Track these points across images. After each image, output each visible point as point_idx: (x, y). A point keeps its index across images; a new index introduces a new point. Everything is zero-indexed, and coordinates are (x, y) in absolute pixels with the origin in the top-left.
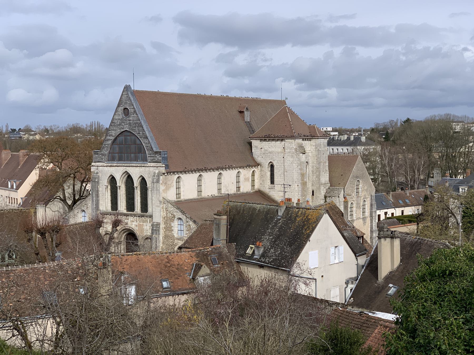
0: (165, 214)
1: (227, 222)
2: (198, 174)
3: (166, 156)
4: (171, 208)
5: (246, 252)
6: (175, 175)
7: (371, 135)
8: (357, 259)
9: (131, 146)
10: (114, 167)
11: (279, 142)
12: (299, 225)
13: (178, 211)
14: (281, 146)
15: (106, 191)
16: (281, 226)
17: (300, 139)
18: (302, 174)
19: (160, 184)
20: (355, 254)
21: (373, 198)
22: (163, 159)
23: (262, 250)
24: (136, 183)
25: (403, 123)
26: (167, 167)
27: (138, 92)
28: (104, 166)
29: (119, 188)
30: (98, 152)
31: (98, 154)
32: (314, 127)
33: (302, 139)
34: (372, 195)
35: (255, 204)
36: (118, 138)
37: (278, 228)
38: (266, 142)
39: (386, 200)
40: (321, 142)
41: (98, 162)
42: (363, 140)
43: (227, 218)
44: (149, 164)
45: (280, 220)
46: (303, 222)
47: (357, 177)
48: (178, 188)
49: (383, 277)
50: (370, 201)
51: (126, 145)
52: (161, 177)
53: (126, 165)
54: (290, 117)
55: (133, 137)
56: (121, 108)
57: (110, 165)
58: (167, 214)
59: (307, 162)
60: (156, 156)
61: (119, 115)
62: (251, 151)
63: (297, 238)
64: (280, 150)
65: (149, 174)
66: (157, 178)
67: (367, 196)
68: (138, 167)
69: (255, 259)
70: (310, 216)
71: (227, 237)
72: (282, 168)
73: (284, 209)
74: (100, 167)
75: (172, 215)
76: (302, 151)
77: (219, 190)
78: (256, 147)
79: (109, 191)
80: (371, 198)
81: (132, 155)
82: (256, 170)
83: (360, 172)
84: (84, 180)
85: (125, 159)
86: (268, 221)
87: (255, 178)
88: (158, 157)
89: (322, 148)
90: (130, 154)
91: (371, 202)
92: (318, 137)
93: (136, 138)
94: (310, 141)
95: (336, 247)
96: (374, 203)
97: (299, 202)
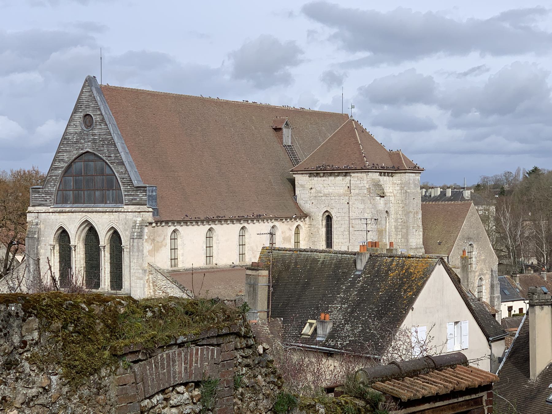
0: (151, 291)
1: (269, 280)
2: (207, 227)
3: (154, 194)
4: (163, 282)
5: (302, 331)
6: (169, 226)
7: (476, 194)
8: (490, 345)
9: (96, 177)
10: (66, 214)
11: (340, 178)
12: (393, 283)
13: (174, 286)
14: (345, 185)
15: (52, 254)
16: (362, 286)
17: (376, 172)
18: (379, 231)
19: (145, 241)
20: (487, 337)
21: (494, 275)
22: (149, 200)
23: (329, 327)
24: (104, 239)
25: (527, 175)
26: (156, 212)
27: (108, 88)
28: (49, 212)
29: (73, 249)
30: (39, 188)
31: (39, 192)
32: (399, 154)
33: (378, 174)
34: (493, 269)
35: (315, 253)
36: (74, 166)
37: (356, 291)
38: (319, 179)
39: (510, 287)
40: (409, 180)
41: (40, 205)
42: (467, 195)
43: (269, 275)
44: (125, 207)
45: (359, 276)
46: (401, 279)
47: (469, 239)
48: (174, 249)
49: (538, 373)
50: (490, 280)
51: (87, 177)
52: (146, 230)
53: (86, 209)
54: (360, 137)
55: (99, 163)
56: (80, 115)
57: (59, 209)
58: (154, 291)
59: (387, 212)
60: (138, 193)
61: (76, 125)
62: (293, 192)
63: (391, 305)
64: (342, 191)
65: (126, 224)
66: (139, 230)
67: (485, 272)
68: (107, 213)
69: (317, 343)
70: (412, 268)
71: (268, 308)
72: (346, 222)
73: (367, 259)
74: (42, 214)
75: (163, 293)
76: (379, 193)
77: (242, 254)
78: (302, 186)
79: (57, 255)
80: (492, 274)
81: (98, 193)
82: (301, 224)
83: (474, 231)
84: (12, 242)
85: (85, 201)
86: (339, 280)
87: (301, 239)
88: (141, 195)
89: (411, 188)
90: (92, 192)
91: (492, 280)
92: (404, 170)
93: (105, 163)
94: (392, 176)
95: (456, 323)
96: (496, 284)
97: (391, 248)
